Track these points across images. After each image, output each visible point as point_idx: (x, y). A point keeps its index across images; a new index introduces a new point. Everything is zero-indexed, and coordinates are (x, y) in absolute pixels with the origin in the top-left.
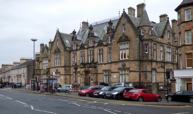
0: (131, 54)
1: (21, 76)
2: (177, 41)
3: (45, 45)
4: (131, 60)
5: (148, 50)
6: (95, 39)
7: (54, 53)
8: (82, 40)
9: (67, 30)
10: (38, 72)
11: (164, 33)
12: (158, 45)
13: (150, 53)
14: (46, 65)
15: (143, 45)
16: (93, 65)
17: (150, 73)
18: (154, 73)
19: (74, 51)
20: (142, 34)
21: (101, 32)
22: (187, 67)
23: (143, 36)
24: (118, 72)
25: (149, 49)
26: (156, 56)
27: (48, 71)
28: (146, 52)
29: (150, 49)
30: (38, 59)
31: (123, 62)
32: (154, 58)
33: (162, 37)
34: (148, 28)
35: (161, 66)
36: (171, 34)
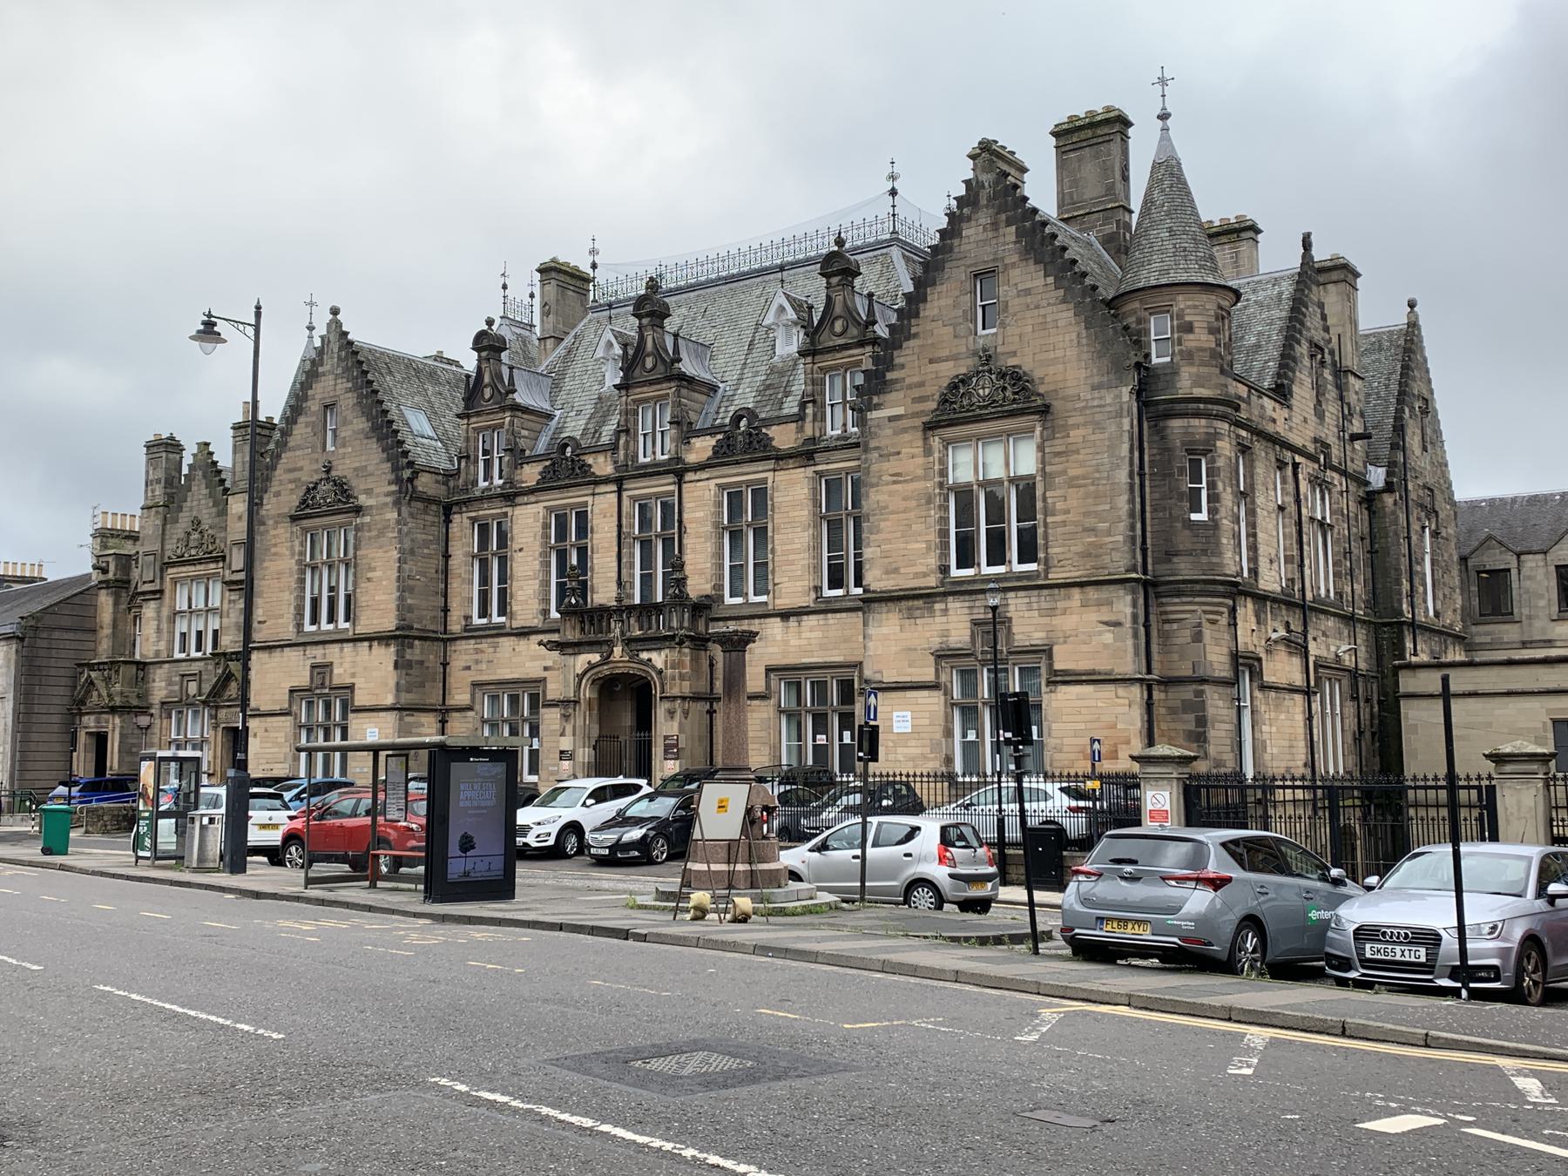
0: (1064, 524)
2: (1354, 437)
4: (1056, 576)
5: (1214, 498)
6: (693, 400)
7: (294, 519)
8: (557, 413)
15: (1166, 450)
17: (1221, 689)
19: (481, 499)
20: (1155, 360)
23: (1172, 371)
24: (934, 686)
25: (1220, 486)
27: (227, 678)
30: (122, 574)
33: (1281, 393)
34: (1210, 302)
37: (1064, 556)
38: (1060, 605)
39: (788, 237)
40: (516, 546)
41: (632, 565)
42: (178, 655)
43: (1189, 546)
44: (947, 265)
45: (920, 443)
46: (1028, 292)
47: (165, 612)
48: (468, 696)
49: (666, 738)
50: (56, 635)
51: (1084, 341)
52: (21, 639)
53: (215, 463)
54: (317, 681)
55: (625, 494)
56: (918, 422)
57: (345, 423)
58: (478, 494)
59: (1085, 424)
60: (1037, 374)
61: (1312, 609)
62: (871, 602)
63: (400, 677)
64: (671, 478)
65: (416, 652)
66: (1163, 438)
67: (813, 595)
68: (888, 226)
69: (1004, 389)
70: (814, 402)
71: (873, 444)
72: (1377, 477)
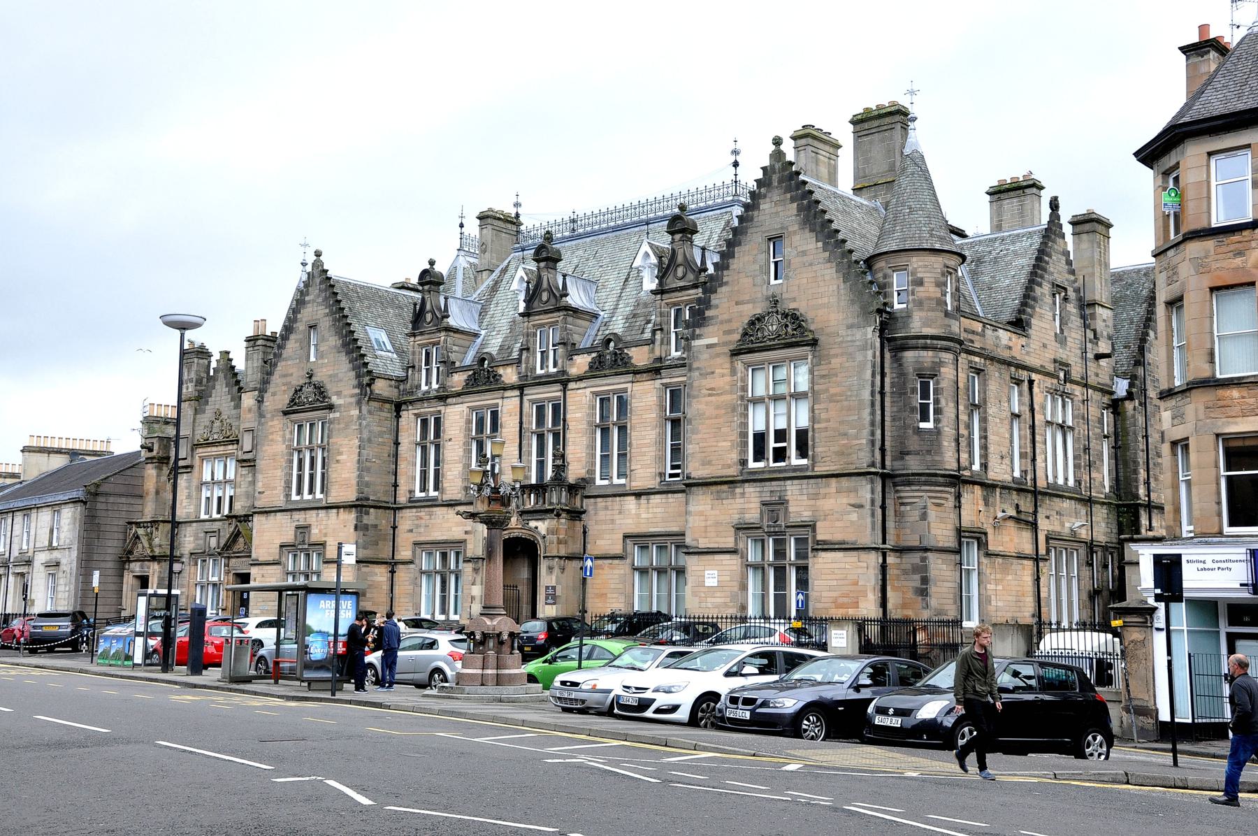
1: (29, 563)
3: (216, 356)
4: (820, 469)
5: (938, 411)
7: (285, 413)
8: (483, 332)
9: (377, 261)
10: (157, 541)
11: (1028, 298)
12: (996, 378)
13: (948, 431)
14: (217, 493)
15: (902, 374)
16: (557, 498)
17: (944, 556)
18: (973, 554)
19: (421, 400)
20: (897, 306)
21: (613, 282)
22: (1231, 524)
24: (734, 552)
25: (943, 402)
26: (984, 448)
27: (236, 536)
28: (925, 418)
29: (952, 405)
30: (166, 448)
31: (768, 486)
32: (971, 463)
33: (1019, 324)
34: (938, 262)
35: (1014, 513)
36: (1072, 308)
37: (827, 456)
38: (823, 491)
39: (668, 195)
40: (447, 437)
41: (530, 454)
42: (203, 517)
43: (917, 448)
44: (750, 231)
45: (728, 365)
46: (804, 253)
47: (195, 482)
48: (733, 539)
49: (547, 588)
50: (111, 499)
51: (842, 292)
52: (85, 503)
53: (233, 368)
54: (300, 539)
55: (525, 398)
56: (726, 350)
57: (323, 340)
58: (420, 395)
59: (842, 355)
60: (809, 316)
61: (1045, 494)
62: (691, 485)
63: (358, 537)
64: (558, 387)
65: (372, 517)
66: (901, 365)
67: (658, 480)
68: (732, 190)
69: (787, 326)
70: (661, 330)
71: (695, 366)
72: (1121, 387)
